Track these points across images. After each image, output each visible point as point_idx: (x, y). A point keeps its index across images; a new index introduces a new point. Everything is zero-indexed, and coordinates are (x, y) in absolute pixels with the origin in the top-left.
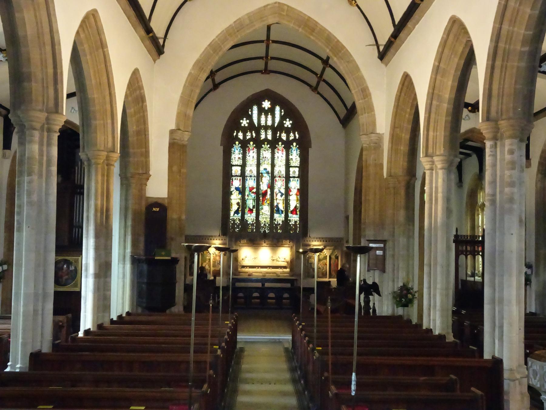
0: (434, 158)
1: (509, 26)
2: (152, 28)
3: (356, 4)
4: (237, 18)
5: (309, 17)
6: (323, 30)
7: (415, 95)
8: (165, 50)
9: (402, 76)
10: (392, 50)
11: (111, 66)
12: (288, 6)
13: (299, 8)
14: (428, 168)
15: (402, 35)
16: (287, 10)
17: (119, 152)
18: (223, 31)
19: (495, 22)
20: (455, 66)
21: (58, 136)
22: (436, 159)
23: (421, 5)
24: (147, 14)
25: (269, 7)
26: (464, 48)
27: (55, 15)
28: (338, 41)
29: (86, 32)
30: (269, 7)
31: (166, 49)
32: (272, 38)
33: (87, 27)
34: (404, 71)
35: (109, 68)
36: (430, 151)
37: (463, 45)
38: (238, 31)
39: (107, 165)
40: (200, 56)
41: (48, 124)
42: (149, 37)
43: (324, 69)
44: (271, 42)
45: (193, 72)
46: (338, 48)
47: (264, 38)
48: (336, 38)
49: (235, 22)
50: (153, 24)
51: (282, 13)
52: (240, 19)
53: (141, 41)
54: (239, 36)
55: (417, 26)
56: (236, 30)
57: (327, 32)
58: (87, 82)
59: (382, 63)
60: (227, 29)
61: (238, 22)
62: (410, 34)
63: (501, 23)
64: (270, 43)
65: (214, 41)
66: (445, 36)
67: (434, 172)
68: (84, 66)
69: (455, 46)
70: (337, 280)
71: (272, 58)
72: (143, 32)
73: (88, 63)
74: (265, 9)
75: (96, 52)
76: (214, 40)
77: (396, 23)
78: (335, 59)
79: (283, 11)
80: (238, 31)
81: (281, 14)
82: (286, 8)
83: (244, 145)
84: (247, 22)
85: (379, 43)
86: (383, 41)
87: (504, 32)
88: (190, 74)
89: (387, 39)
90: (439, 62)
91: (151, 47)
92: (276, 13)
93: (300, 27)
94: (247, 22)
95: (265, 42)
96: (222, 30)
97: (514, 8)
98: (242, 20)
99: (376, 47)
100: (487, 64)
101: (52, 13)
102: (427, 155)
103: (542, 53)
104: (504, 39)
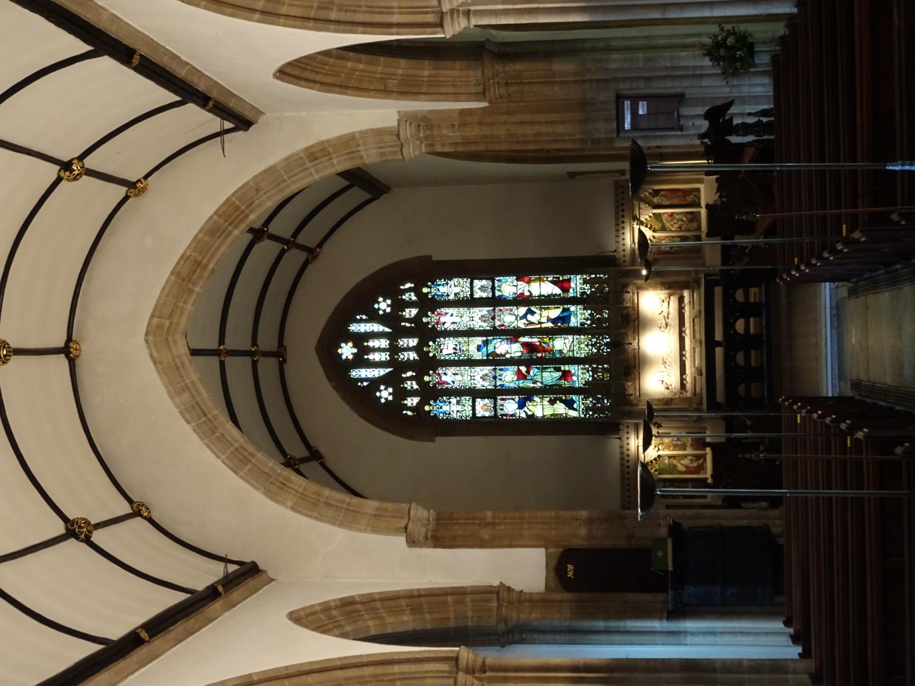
0: (444, 10)
2: (208, 588)
3: (142, 180)
5: (172, 273)
6: (197, 243)
9: (283, 80)
10: (232, 104)
11: (286, 668)
12: (152, 316)
15: (202, 86)
16: (160, 317)
18: (206, 445)
23: (142, 54)
30: (155, 355)
32: (213, 344)
38: (205, 415)
39: (485, 672)
44: (222, 347)
45: (290, 504)
47: (215, 360)
49: (188, 422)
52: (181, 413)
54: (215, 412)
55: (184, 58)
56: (204, 419)
57: (201, 235)
59: (256, 123)
60: (203, 436)
61: (188, 417)
62: (199, 71)
72: (217, 605)
74: (161, 363)
77: (178, 99)
78: (252, 217)
79: (160, 326)
80: (205, 415)
82: (155, 321)
84: (186, 396)
88: (293, 509)
90: (254, 11)
96: (205, 448)
98: (183, 407)
102: (440, 25)
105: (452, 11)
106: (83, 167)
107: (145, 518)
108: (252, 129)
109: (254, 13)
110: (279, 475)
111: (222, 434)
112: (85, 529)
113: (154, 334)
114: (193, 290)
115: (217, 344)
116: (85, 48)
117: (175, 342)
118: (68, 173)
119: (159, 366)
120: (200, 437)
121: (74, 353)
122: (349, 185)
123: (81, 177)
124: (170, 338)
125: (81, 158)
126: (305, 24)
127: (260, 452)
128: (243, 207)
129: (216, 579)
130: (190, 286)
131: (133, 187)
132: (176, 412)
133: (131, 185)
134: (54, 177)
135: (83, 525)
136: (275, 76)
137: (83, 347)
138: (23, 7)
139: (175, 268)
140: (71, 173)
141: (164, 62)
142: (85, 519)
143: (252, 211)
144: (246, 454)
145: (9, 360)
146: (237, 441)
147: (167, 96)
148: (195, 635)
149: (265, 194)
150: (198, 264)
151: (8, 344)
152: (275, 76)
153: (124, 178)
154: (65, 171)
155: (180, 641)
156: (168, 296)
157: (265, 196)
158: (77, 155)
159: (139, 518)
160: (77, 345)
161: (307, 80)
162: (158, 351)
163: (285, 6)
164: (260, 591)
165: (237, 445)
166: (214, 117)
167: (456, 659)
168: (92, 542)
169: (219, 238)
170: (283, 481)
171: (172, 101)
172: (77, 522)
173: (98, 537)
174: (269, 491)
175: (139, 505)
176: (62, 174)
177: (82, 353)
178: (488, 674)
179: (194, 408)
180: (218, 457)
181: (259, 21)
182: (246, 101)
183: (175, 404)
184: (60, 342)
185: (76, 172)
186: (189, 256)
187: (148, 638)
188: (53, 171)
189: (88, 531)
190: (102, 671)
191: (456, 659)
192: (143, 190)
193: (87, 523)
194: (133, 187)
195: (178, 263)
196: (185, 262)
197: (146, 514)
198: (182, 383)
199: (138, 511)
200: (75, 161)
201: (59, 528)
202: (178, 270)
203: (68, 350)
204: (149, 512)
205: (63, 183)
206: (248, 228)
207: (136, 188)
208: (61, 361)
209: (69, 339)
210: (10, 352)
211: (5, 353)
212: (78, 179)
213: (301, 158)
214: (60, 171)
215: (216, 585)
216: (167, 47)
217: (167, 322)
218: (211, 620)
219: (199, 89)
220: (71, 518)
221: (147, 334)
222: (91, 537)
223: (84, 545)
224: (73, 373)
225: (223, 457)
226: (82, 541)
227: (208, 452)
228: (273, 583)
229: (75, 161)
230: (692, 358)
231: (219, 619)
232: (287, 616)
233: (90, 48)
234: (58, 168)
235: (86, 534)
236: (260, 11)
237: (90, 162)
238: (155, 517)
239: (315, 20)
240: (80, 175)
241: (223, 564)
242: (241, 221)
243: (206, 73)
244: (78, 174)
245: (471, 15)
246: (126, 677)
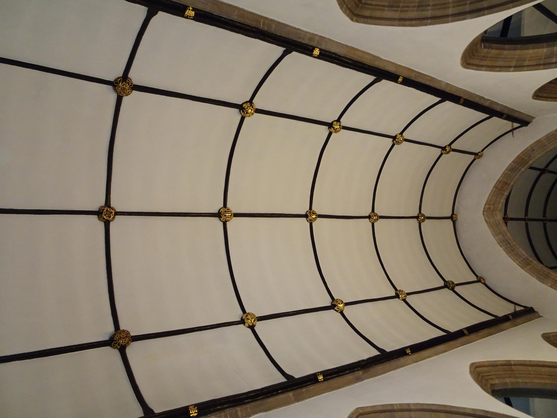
1: (449, 8)
2: (504, 316)
3: (481, 152)
4: (498, 244)
5: (494, 187)
6: (504, 174)
8: (529, 306)
9: (538, 100)
10: (516, 115)
11: (530, 361)
12: (486, 205)
13: (487, 195)
15: (498, 109)
16: (489, 205)
18: (509, 256)
19: (447, 22)
20: (512, 52)
23: (465, 98)
24: (489, 318)
25: (487, 220)
26: (492, 49)
27: (457, 408)
28: (513, 162)
29: (494, 377)
30: (487, 220)
31: (529, 305)
32: (522, 216)
33: (488, 375)
34: (461, 68)
35: (532, 363)
37: (490, 50)
38: (509, 244)
40: (534, 276)
42: (513, 318)
43: (550, 172)
44: (526, 217)
45: (550, 284)
46: (520, 161)
47: (523, 223)
48: (510, 164)
49: (501, 247)
50: (501, 314)
51: (492, 209)
52: (498, 243)
53: (516, 327)
54: (514, 243)
55: (486, 97)
56: (509, 246)
57: (506, 172)
58: (549, 387)
59: (531, 122)
60: (508, 252)
61: (501, 244)
62: (496, 102)
63: (448, 16)
64: (528, 218)
65: (519, 264)
66: (549, 99)
68: (529, 386)
69: (491, 58)
71: (544, 215)
72: (508, 324)
73: (526, 383)
74: (489, 223)
75: (515, 372)
76: (517, 264)
77: (488, 116)
78: (531, 162)
79: (489, 208)
80: (509, 244)
81: (493, 210)
82: (487, 206)
84: (500, 236)
85: (510, 129)
86: (507, 125)
87: (456, 10)
88: (551, 287)
89: (506, 122)
90: (510, 67)
91: (523, 318)
92: (492, 214)
93: (503, 194)
94: (500, 236)
95: (527, 222)
96: (508, 257)
97: (432, 10)
98: (499, 241)
99: (514, 131)
100: (488, 14)
101: (455, 410)
104: (462, 7)
106: (450, 148)
107: (483, 283)
108: (529, 125)
109: (511, 68)
110: (545, 271)
111: (517, 252)
112: (451, 285)
113: (487, 212)
114: (504, 194)
115: (524, 215)
116: (438, 99)
117: (496, 214)
118: (444, 151)
119: (489, 224)
120: (506, 253)
121: (454, 219)
122: (520, 126)
123: (450, 152)
124: (494, 213)
125: (450, 145)
126: (539, 67)
127: (535, 261)
128: (526, 158)
129: (509, 312)
130: (503, 192)
131: (477, 155)
132: (495, 242)
133: (476, 154)
135: (451, 284)
136: (533, 98)
137: (459, 217)
138: (195, 21)
139: (495, 185)
140: (446, 151)
141: (477, 100)
142: (452, 281)
143: (530, 160)
144: (528, 261)
145: (425, 221)
146: (524, 255)
148: (493, 336)
149: (536, 151)
150: (506, 183)
151: (424, 215)
152: (533, 98)
153: (387, 134)
154: (443, 151)
155: (485, 337)
156: (493, 196)
157: (536, 153)
158: (448, 144)
159: (480, 283)
160: (456, 216)
161: (552, 98)
162: (488, 218)
163: (527, 61)
164: (533, 321)
165: (524, 257)
166: (509, 122)
168: (454, 290)
169: (515, 172)
170: (546, 274)
171: (486, 117)
172: (449, 282)
173: (457, 289)
174: (539, 278)
175: (480, 278)
176: (442, 152)
177: (458, 219)
179: (504, 241)
180: (515, 262)
181: (514, 71)
183: (495, 239)
184: (449, 214)
185: (448, 151)
186: (502, 180)
187: (468, 334)
188: (439, 151)
189: (453, 286)
190: (442, 344)
192: (481, 156)
193: (453, 283)
194: (477, 155)
195: (496, 183)
196: (500, 183)
197: (483, 282)
198: (499, 231)
199: (479, 280)
202: (496, 186)
203: (453, 218)
204: (485, 281)
205: (444, 155)
206: (529, 167)
207: (478, 155)
208: (450, 222)
209: (453, 213)
210: (425, 218)
211: (423, 218)
212: (449, 153)
213: (554, 134)
214: (441, 151)
215: (508, 315)
216: (476, 94)
217: (492, 207)
218: (503, 330)
219: (497, 110)
220: (447, 280)
221: (483, 212)
222: (454, 288)
223: (451, 291)
224: (135, 214)
225: (517, 262)
226: (450, 290)
227: (510, 258)
228: (541, 318)
229: (335, 123)
231: (507, 330)
232: (541, 335)
233: (440, 99)
234: (441, 149)
235: (452, 287)
236: (513, 66)
237: (454, 146)
238: (487, 283)
239: (544, 64)
240: (449, 151)
241: (514, 305)
242: (526, 164)
243: (499, 103)
244: (448, 151)
246: (453, 349)
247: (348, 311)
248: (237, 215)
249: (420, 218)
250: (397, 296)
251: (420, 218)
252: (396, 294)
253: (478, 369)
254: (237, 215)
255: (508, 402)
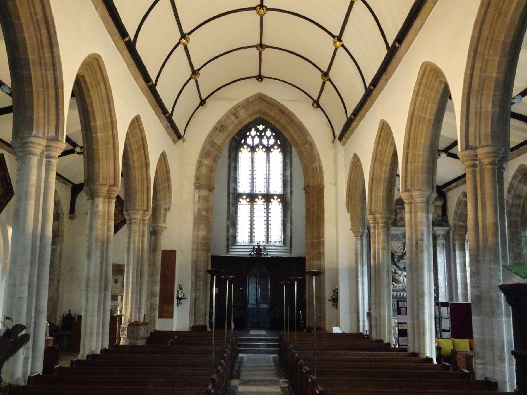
0: (478, 150)
7: (362, 171)
14: (407, 203)
17: (151, 211)
21: (116, 201)
22: (415, 193)
36: (409, 187)
39: (143, 220)
41: (109, 194)
67: (413, 205)
70: (97, 354)
83: (253, 149)
102: (371, 213)
103: (451, 150)
105: (412, 196)
125: (343, 46)
134: (322, 69)
136: (381, 120)
147: (369, 80)
152: (381, 120)
158: (345, 45)
167: (115, 185)
173: (193, 81)
178: (44, 160)
182: (433, 8)
191: (148, 210)
194: (316, 104)
199: (203, 102)
200: (341, 43)
201: (196, 68)
230: (171, 130)
245: (473, 168)
247: (193, 81)
248: (260, 53)
249: (261, 46)
250: (184, 36)
251: (261, 46)
252: (185, 34)
253: (95, 63)
254: (260, 53)
255: (73, 95)
